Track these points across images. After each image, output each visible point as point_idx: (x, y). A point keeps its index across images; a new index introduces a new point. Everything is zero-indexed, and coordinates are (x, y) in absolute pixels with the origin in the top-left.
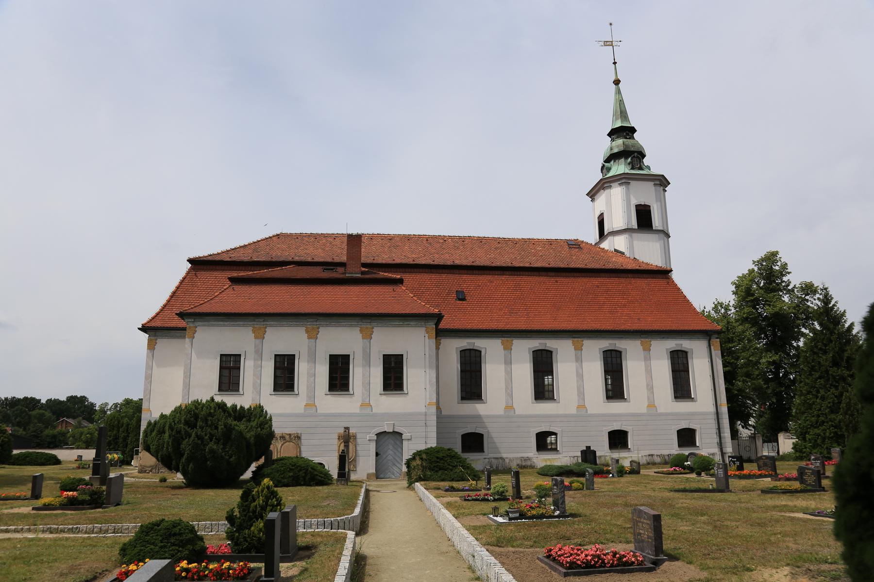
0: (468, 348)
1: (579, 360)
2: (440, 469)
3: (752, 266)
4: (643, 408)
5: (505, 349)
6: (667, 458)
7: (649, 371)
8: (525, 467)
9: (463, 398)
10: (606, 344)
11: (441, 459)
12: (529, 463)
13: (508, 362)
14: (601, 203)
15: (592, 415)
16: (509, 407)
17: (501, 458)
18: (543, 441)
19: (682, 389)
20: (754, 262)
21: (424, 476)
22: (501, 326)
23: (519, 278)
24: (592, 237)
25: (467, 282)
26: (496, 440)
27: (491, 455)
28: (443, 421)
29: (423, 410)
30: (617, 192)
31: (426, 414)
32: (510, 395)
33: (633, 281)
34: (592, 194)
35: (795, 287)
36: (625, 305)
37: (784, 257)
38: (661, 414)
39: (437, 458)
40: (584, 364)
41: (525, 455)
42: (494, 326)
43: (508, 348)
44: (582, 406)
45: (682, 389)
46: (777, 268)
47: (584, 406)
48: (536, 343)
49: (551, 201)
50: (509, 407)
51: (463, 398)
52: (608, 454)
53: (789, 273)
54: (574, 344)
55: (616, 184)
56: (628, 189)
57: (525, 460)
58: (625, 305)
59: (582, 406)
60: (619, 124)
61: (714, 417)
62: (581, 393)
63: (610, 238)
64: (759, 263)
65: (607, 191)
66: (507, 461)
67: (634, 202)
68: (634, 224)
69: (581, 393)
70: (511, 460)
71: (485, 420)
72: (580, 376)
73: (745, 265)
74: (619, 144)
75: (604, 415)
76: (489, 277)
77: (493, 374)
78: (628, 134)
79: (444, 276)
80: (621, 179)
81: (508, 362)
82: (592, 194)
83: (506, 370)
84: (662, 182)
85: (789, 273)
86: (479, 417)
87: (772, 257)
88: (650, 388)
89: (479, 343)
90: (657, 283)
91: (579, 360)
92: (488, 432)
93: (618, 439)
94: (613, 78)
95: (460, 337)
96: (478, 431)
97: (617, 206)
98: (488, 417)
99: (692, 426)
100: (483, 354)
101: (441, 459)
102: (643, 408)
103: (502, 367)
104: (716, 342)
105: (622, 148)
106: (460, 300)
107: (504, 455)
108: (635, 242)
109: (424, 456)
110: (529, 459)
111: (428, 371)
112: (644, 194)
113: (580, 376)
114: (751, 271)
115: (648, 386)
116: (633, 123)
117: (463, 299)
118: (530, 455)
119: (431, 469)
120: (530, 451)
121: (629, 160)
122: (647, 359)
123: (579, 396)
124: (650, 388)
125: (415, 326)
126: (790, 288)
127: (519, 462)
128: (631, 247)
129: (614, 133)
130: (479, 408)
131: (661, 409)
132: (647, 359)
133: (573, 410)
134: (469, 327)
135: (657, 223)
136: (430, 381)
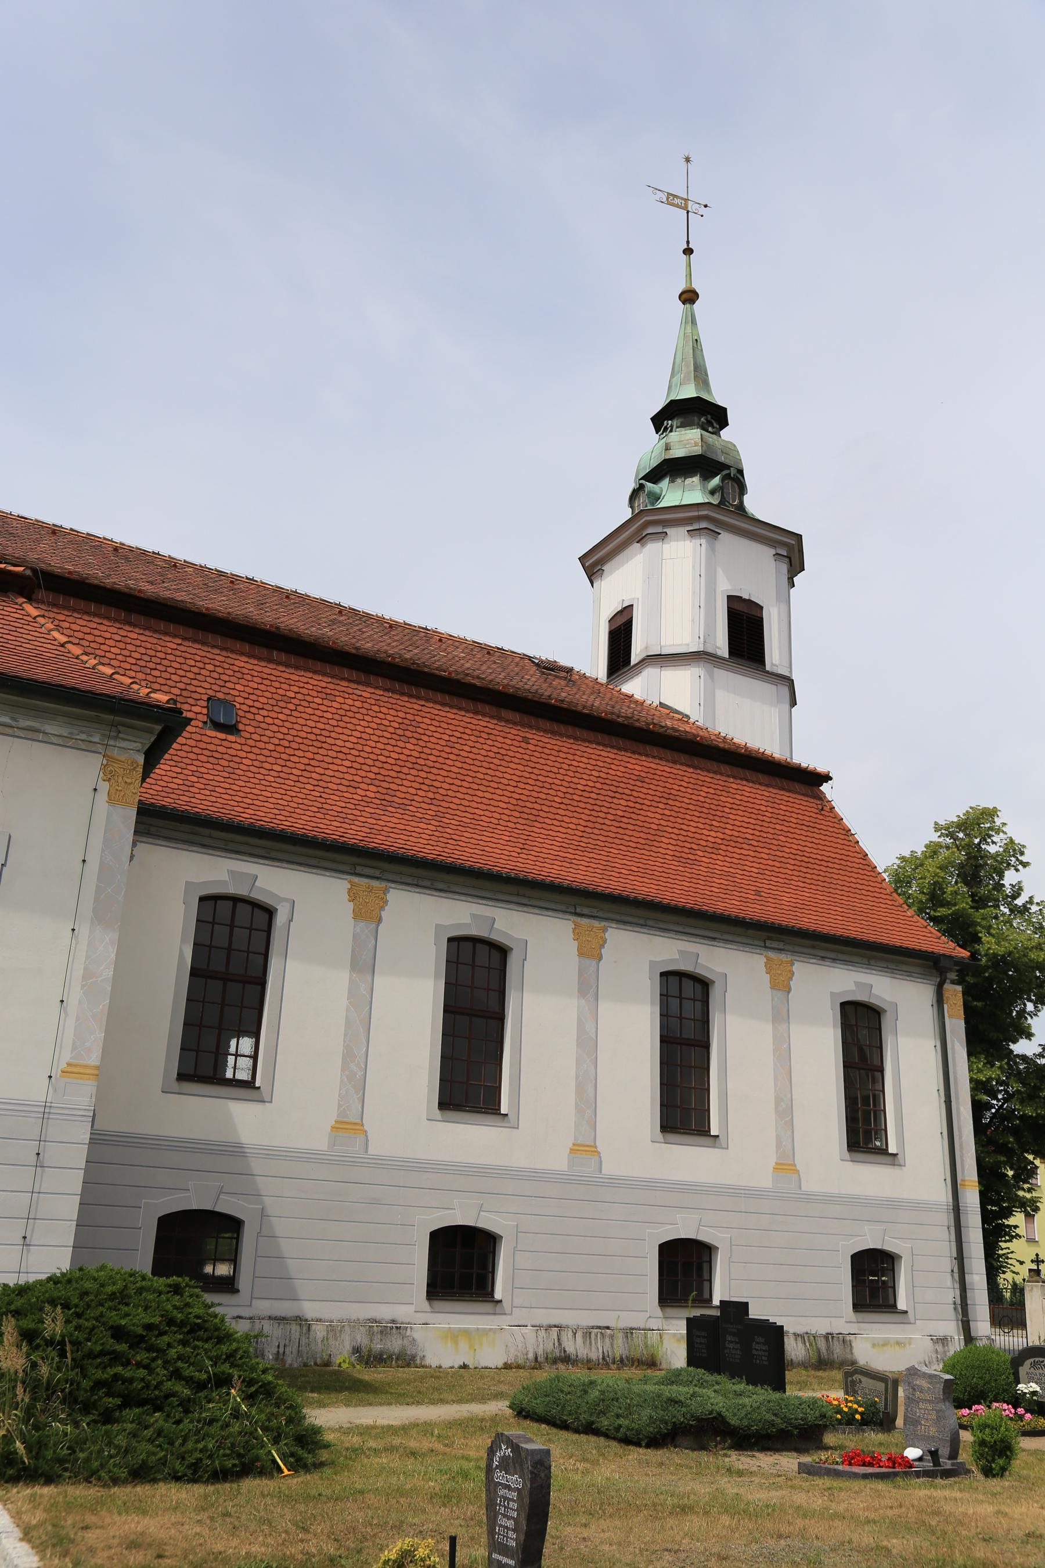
0: (231, 890)
1: (588, 989)
2: (128, 1401)
3: (935, 837)
4: (761, 1175)
5: (357, 915)
6: (822, 1344)
7: (783, 1054)
8: (377, 1359)
9: (182, 1077)
10: (671, 950)
11: (137, 1341)
12: (394, 1344)
13: (364, 964)
14: (625, 581)
15: (615, 1183)
16: (349, 1126)
17: (299, 1320)
18: (462, 1263)
19: (864, 1128)
20: (937, 827)
21: (36, 1448)
22: (354, 834)
23: (416, 705)
24: (593, 663)
25: (246, 678)
26: (287, 1247)
27: (264, 1307)
28: (111, 1154)
29: (37, 1091)
30: (680, 555)
31: (46, 1112)
32: (356, 1080)
33: (734, 785)
34: (595, 563)
35: (1031, 901)
36: (715, 848)
37: (1014, 825)
38: (811, 1198)
39: (118, 1333)
40: (604, 1007)
41: (385, 1312)
42: (330, 829)
43: (368, 914)
44: (585, 1149)
45: (864, 1128)
46: (992, 849)
47: (591, 1149)
48: (464, 914)
49: (492, 550)
50: (349, 1126)
51: (182, 1077)
52: (654, 1324)
53: (1025, 865)
54: (577, 935)
55: (682, 531)
56: (712, 549)
57: (385, 1332)
58: (715, 848)
59: (585, 1149)
60: (689, 392)
61: (945, 1218)
62: (587, 1104)
63: (650, 672)
64: (948, 830)
65: (652, 547)
66: (319, 1331)
67: (725, 587)
68: (721, 644)
69: (587, 1104)
70: (334, 1329)
71: (257, 1166)
72: (588, 1044)
73: (953, 813)
74: (686, 440)
75: (650, 1185)
76: (320, 681)
77: (304, 990)
78: (710, 424)
79: (171, 643)
80: (699, 518)
81: (364, 964)
82: (595, 563)
83: (352, 993)
84: (789, 550)
85: (1025, 865)
86: (235, 1151)
87: (978, 823)
88: (785, 1110)
89: (270, 880)
90: (788, 802)
91: (588, 989)
92: (263, 1214)
93: (462, 1263)
94: (682, 286)
95: (206, 846)
96: (226, 1206)
97: (676, 590)
98: (270, 1154)
99: (890, 1245)
100: (280, 919)
101: (137, 1341)
102: (761, 1175)
103: (341, 979)
104: (954, 993)
105: (697, 450)
106: (218, 726)
107: (310, 1310)
108: (720, 694)
109: (54, 1325)
110: (396, 1327)
111: (84, 931)
112: (752, 573)
113: (588, 1044)
114: (933, 850)
115: (778, 1100)
116: (718, 397)
117: (231, 729)
118: (402, 1312)
119: (78, 1404)
120: (397, 1290)
121: (716, 481)
122: (781, 1017)
123: (579, 1111)
124: (785, 1110)
125: (65, 743)
126: (1019, 902)
127: (361, 1338)
128: (709, 703)
129: (671, 414)
130: (244, 1120)
131: (811, 1184)
132: (781, 1017)
133: (557, 1160)
134: (246, 816)
135: (774, 656)
136: (87, 974)
